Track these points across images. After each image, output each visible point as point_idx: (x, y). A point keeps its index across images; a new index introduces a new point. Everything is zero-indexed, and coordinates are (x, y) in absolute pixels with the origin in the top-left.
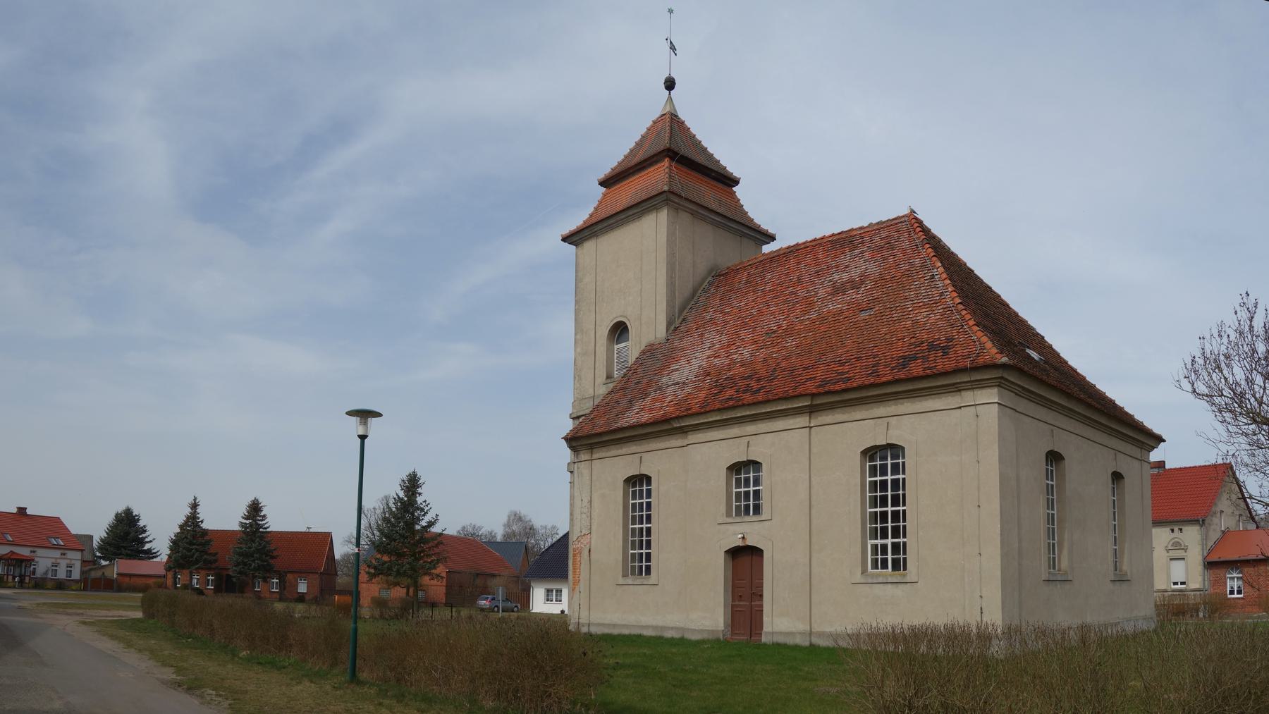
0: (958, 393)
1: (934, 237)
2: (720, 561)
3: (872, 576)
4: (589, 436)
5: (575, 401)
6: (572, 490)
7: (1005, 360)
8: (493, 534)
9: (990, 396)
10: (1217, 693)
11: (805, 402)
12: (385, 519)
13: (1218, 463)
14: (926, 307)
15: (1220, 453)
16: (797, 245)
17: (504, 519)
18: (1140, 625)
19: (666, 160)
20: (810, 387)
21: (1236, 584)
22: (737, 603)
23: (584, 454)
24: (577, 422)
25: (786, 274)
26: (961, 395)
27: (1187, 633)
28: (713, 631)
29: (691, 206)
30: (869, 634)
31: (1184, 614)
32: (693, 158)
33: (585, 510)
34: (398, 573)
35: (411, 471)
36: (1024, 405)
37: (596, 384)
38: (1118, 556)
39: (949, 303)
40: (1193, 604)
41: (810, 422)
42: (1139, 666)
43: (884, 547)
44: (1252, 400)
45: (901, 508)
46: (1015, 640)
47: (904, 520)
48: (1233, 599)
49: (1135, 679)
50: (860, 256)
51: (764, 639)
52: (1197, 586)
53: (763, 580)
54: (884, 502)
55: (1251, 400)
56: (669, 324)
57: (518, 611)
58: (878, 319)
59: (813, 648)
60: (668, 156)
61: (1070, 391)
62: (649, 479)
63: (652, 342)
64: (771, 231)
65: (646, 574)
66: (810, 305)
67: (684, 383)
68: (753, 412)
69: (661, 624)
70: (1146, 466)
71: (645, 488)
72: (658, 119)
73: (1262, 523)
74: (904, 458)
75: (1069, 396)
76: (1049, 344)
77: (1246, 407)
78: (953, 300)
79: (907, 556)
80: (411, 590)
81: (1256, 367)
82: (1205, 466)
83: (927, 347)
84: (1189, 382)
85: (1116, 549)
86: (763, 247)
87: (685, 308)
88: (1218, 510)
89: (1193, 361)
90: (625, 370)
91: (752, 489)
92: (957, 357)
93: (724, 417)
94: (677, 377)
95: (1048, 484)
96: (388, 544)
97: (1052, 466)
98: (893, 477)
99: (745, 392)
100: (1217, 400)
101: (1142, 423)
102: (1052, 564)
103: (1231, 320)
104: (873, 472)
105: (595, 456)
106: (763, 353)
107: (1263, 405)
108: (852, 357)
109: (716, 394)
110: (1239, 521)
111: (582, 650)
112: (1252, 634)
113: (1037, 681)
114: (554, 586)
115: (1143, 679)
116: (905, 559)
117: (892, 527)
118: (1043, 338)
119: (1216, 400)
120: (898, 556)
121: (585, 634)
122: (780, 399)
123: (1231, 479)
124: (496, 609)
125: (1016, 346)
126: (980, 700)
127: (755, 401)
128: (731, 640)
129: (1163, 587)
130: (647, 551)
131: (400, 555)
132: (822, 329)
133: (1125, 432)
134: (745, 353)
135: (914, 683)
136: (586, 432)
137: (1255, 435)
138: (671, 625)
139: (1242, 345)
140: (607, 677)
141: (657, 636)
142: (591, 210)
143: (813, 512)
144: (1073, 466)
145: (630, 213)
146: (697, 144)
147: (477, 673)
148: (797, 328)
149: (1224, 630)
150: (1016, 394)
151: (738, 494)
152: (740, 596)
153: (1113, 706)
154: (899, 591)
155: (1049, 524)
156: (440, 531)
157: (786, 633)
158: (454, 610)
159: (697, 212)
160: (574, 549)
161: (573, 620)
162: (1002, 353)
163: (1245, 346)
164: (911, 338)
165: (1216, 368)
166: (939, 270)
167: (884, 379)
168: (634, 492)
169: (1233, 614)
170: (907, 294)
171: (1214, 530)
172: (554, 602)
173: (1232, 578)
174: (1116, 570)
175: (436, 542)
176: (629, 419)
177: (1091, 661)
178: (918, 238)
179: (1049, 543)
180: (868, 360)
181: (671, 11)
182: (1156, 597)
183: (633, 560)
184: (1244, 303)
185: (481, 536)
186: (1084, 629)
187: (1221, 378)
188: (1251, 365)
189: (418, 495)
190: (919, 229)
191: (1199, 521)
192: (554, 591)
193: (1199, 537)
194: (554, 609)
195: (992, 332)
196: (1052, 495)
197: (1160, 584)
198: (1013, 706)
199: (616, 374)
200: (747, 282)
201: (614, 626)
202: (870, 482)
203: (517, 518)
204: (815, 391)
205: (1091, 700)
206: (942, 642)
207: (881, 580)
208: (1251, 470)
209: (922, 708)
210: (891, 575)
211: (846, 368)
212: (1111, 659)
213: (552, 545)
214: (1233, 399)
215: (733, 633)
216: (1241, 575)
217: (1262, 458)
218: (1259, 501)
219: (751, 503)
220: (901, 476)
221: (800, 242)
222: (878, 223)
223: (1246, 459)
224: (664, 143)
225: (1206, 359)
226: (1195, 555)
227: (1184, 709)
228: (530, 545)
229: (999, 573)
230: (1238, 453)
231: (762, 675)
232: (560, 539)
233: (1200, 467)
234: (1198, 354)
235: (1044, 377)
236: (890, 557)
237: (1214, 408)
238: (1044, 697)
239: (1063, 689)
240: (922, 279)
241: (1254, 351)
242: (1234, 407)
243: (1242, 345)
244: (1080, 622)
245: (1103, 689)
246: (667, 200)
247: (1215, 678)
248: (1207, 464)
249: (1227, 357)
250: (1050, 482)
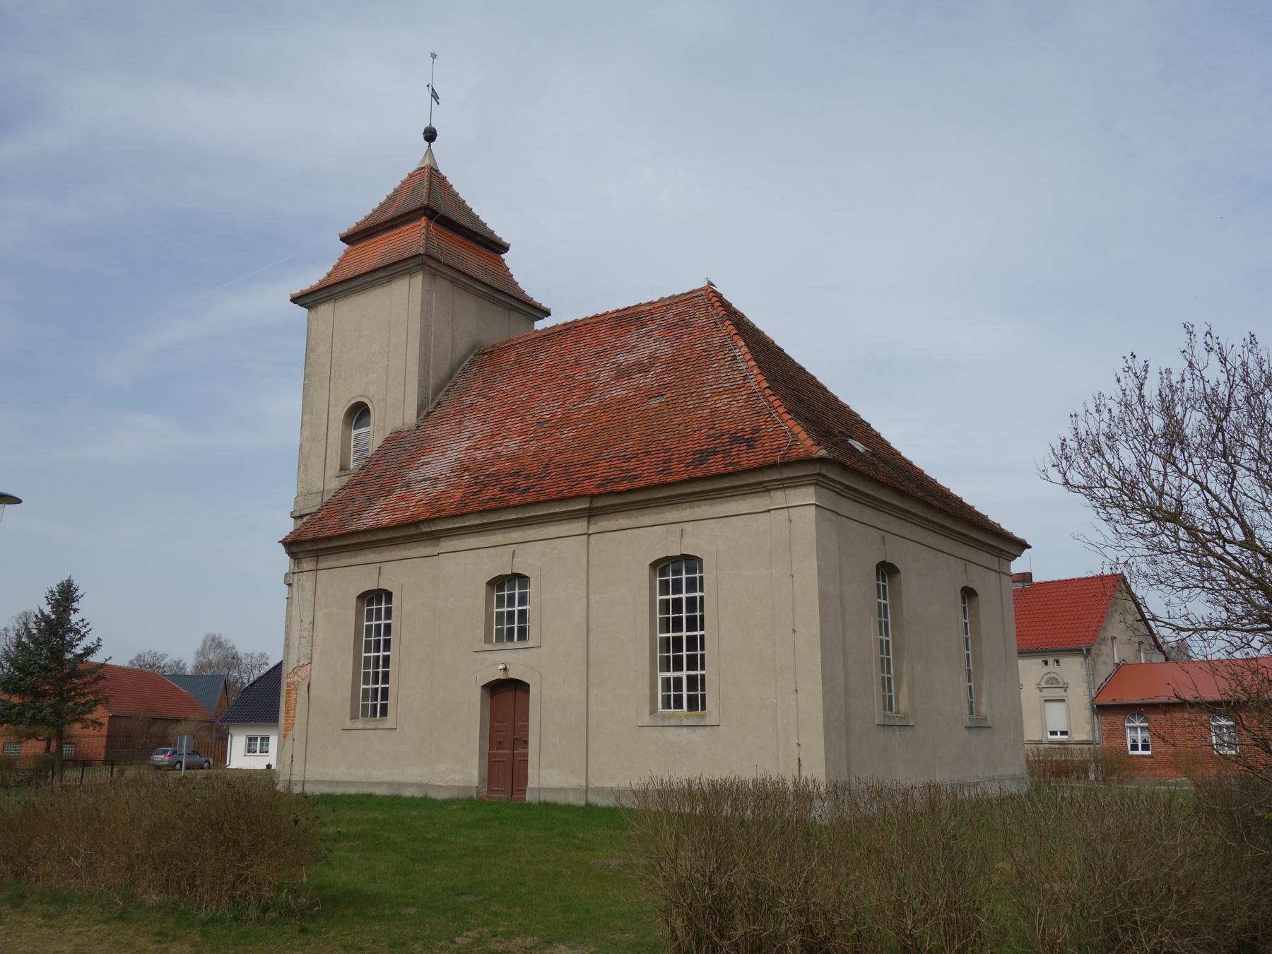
0: (767, 493)
1: (736, 312)
2: (475, 697)
3: (664, 717)
4: (314, 541)
6: (289, 608)
7: (823, 453)
8: (181, 665)
9: (807, 495)
10: (1121, 886)
11: (584, 505)
12: (19, 644)
13: (1105, 573)
14: (727, 392)
15: (1107, 561)
16: (576, 321)
17: (198, 645)
18: (1008, 786)
19: (423, 218)
20: (590, 487)
21: (1140, 737)
22: (496, 751)
23: (306, 562)
24: (300, 522)
25: (562, 355)
26: (770, 495)
27: (1072, 801)
28: (464, 787)
29: (451, 273)
30: (659, 791)
31: (1067, 774)
32: (455, 219)
33: (306, 634)
34: (34, 720)
35: (65, 579)
36: (847, 507)
37: (327, 477)
38: (973, 696)
39: (754, 387)
40: (1080, 762)
41: (588, 529)
42: (1008, 842)
43: (678, 682)
44: (1149, 490)
45: (698, 633)
46: (843, 802)
47: (702, 648)
48: (1137, 756)
49: (1003, 860)
50: (649, 334)
51: (529, 797)
52: (1084, 737)
53: (528, 721)
54: (677, 625)
55: (1147, 491)
56: (421, 408)
57: (209, 767)
58: (670, 406)
59: (589, 809)
60: (426, 215)
61: (904, 489)
62: (389, 596)
63: (399, 429)
64: (545, 305)
65: (381, 716)
66: (590, 390)
67: (437, 479)
68: (520, 516)
69: (397, 779)
70: (1006, 580)
71: (383, 606)
72: (414, 172)
73: (1173, 654)
74: (701, 571)
75: (903, 494)
76: (876, 433)
77: (1141, 500)
78: (759, 384)
79: (707, 693)
80: (53, 744)
81: (1151, 447)
82: (1087, 578)
83: (727, 440)
84: (1060, 471)
85: (970, 687)
86: (536, 323)
87: (440, 390)
88: (1109, 635)
89: (1063, 444)
90: (364, 461)
91: (517, 608)
92: (765, 450)
93: (485, 521)
94: (429, 472)
95: (880, 604)
96: (21, 679)
97: (884, 581)
98: (689, 595)
99: (511, 491)
100: (1099, 492)
101: (999, 525)
102: (888, 704)
103: (1112, 391)
104: (664, 588)
105: (321, 566)
106: (533, 446)
107: (1165, 496)
108: (639, 452)
109: (475, 493)
110: (1139, 650)
111: (292, 817)
112: (1168, 807)
113: (873, 857)
114: (258, 732)
115: (1014, 860)
116: (703, 697)
117: (687, 656)
118: (869, 425)
119: (1097, 493)
120: (696, 693)
121: (298, 795)
122: (553, 500)
123: (1125, 595)
124: (178, 766)
125: (836, 436)
126: (800, 878)
127: (523, 502)
128: (488, 800)
129: (1037, 738)
130: (384, 686)
131: (38, 695)
132: (604, 419)
133: (975, 536)
134: (513, 445)
135: (716, 854)
136: (311, 535)
137: (1155, 535)
138: (413, 781)
139: (1130, 421)
140: (324, 851)
141: (392, 796)
142: (330, 269)
143: (591, 636)
144: (911, 582)
145: (378, 275)
146: (461, 204)
147: (138, 855)
148: (574, 417)
149: (1126, 799)
150: (837, 493)
151: (500, 615)
152: (500, 742)
153: (975, 895)
154: (696, 736)
155: (882, 653)
156: (102, 661)
157: (558, 789)
158: (116, 769)
159: (458, 279)
160: (289, 685)
161: (283, 778)
162: (818, 445)
163: (1134, 422)
164: (710, 429)
165: (1094, 452)
166: (742, 350)
167: (677, 478)
168: (370, 612)
169: (1138, 778)
170: (705, 378)
171: (1104, 663)
172: (258, 753)
173: (1135, 728)
174: (972, 714)
175: (94, 676)
176: (368, 520)
177: (943, 834)
178: (717, 314)
179: (883, 678)
180: (658, 456)
181: (434, 56)
182: (1028, 750)
183: (365, 698)
184: (1129, 368)
185: (164, 667)
186: (933, 790)
187: (1102, 464)
188: (1145, 445)
189: (72, 612)
190: (717, 304)
191: (1081, 650)
192: (259, 740)
193: (1083, 672)
194: (257, 763)
195: (807, 420)
196: (886, 617)
197: (1032, 732)
198: (842, 888)
199: (352, 465)
200: (515, 363)
201: (338, 783)
202: (660, 600)
203: (216, 643)
204: (594, 491)
205: (945, 885)
206: (750, 802)
207: (673, 722)
208: (1152, 582)
209: (727, 887)
210: (686, 717)
211: (632, 464)
212: (970, 831)
213: (259, 679)
214: (1122, 490)
215: (490, 791)
216: (1146, 724)
217: (1167, 567)
218: (1167, 624)
219: (516, 626)
220: (698, 594)
221: (579, 319)
222: (670, 298)
223: (1145, 568)
224: (422, 199)
225: (1080, 441)
226: (1080, 696)
227: (1075, 905)
228: (232, 679)
229: (821, 715)
230: (1132, 560)
231: (525, 843)
232: (270, 671)
233: (1079, 579)
234: (1069, 435)
235: (872, 473)
236: (685, 693)
237: (1094, 503)
238: (882, 878)
239: (907, 868)
240: (722, 361)
241: (1147, 426)
242: (1123, 501)
243: (1130, 421)
244: (927, 780)
245: (960, 871)
246: (423, 264)
247: (1117, 865)
248: (1090, 575)
249: (1110, 437)
250: (882, 601)
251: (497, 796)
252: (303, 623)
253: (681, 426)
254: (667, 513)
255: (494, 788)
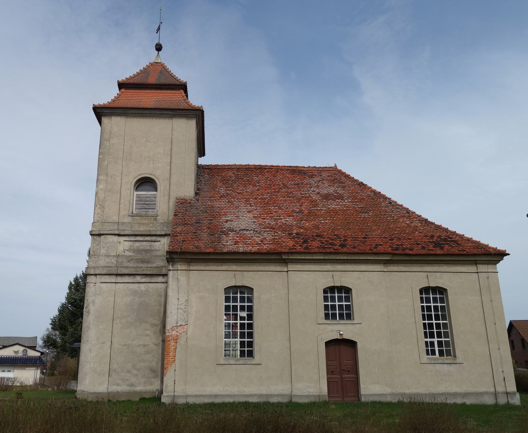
5: (94, 222)
22: (331, 376)
51: (363, 399)
68: (349, 258)
69: (264, 392)
138: (277, 393)
152: (332, 372)
154: (452, 368)
201: (216, 396)
251: (335, 399)
252: (179, 300)
253: (398, 230)
254: (426, 267)
255: (348, 395)
